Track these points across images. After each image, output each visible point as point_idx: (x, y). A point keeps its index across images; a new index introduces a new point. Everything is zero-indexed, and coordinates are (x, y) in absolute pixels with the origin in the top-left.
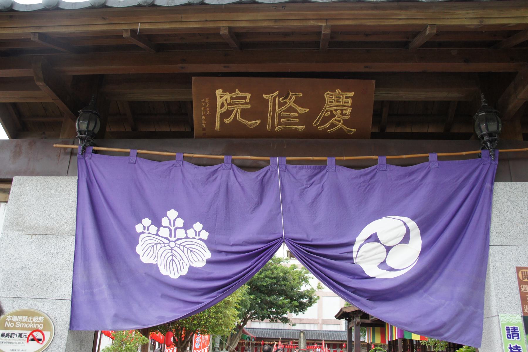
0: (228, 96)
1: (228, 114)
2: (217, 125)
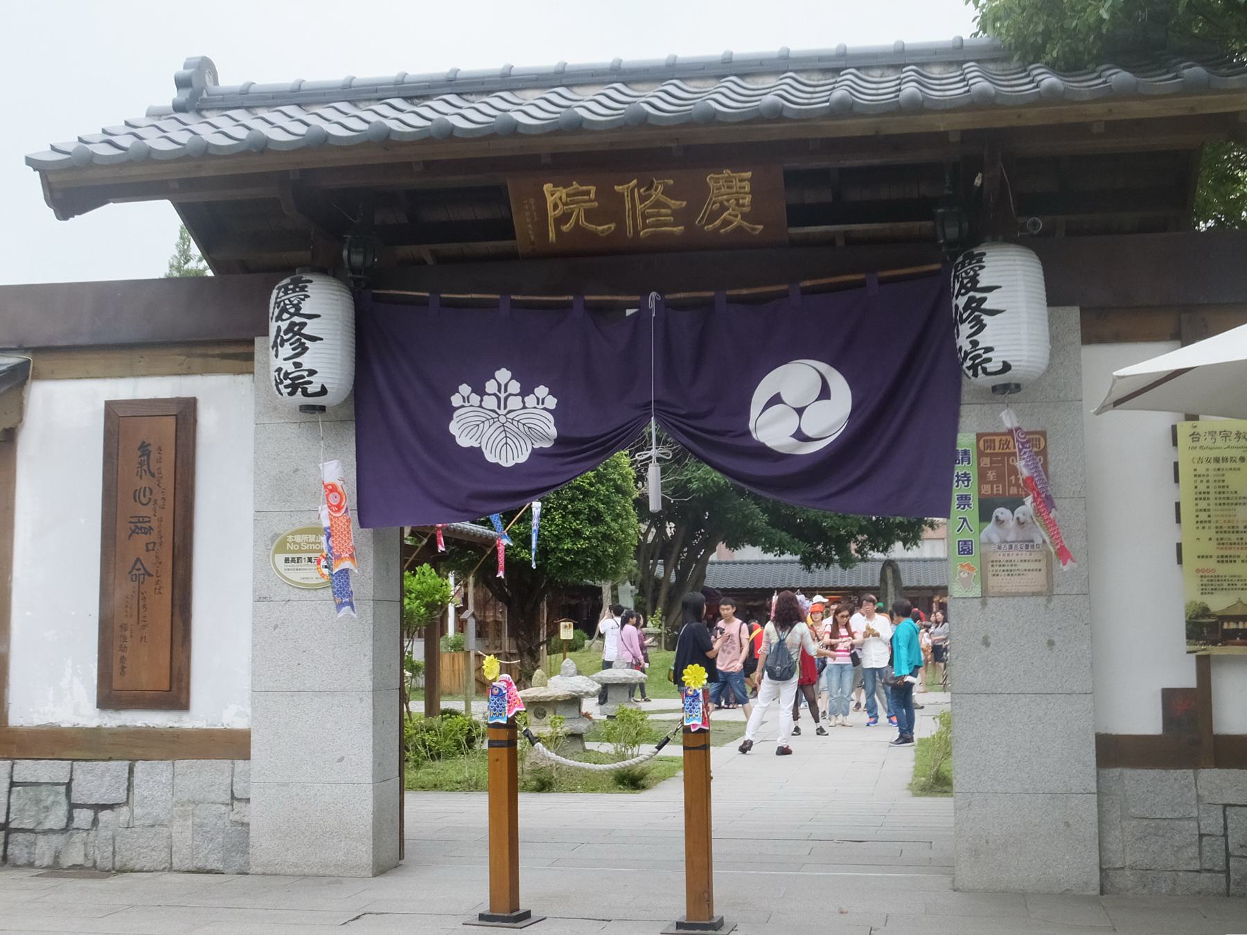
0: (562, 192)
1: (565, 218)
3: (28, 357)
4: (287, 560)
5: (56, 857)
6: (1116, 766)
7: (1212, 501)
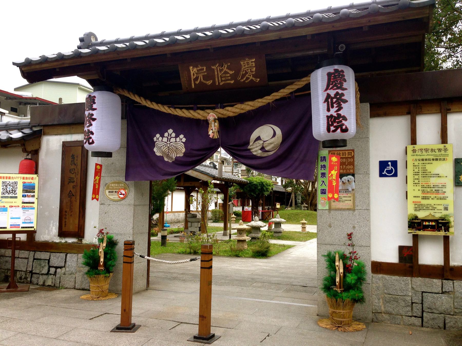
0: (195, 70)
1: (196, 79)
2: (193, 85)
3: (42, 128)
4: (109, 192)
5: (44, 282)
6: (380, 274)
7: (420, 176)
